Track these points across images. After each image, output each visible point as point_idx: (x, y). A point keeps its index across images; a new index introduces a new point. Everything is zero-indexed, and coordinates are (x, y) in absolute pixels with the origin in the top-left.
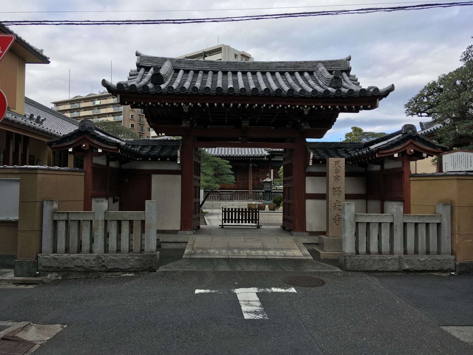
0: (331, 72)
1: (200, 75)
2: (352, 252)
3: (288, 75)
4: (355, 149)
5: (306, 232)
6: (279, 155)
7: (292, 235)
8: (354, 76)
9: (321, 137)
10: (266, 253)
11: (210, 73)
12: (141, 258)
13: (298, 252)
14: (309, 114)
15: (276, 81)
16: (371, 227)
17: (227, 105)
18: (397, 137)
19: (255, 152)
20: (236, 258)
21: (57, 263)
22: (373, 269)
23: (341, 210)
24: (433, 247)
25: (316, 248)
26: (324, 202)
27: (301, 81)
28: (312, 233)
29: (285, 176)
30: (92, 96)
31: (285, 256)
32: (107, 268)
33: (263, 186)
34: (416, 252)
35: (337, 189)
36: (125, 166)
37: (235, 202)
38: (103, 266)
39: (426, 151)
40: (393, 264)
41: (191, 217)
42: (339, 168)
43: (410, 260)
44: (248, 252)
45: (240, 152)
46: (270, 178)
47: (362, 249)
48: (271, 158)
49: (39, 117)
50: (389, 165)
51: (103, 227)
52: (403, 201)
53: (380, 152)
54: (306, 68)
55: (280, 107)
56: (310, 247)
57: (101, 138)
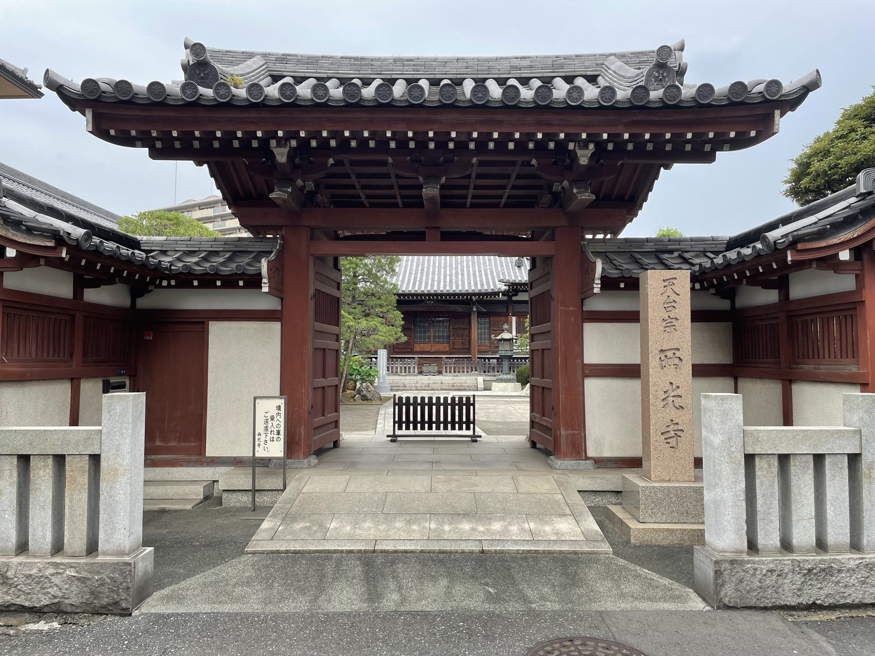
2: (740, 548)
4: (704, 253)
5: (587, 458)
13: (572, 529)
14: (588, 168)
16: (793, 469)
22: (804, 600)
26: (633, 385)
28: (602, 463)
30: (212, 199)
31: (533, 541)
35: (670, 354)
36: (143, 303)
42: (673, 297)
45: (454, 285)
46: (511, 333)
47: (769, 536)
48: (511, 297)
50: (803, 288)
53: (800, 246)
54: (580, 70)
56: (598, 500)
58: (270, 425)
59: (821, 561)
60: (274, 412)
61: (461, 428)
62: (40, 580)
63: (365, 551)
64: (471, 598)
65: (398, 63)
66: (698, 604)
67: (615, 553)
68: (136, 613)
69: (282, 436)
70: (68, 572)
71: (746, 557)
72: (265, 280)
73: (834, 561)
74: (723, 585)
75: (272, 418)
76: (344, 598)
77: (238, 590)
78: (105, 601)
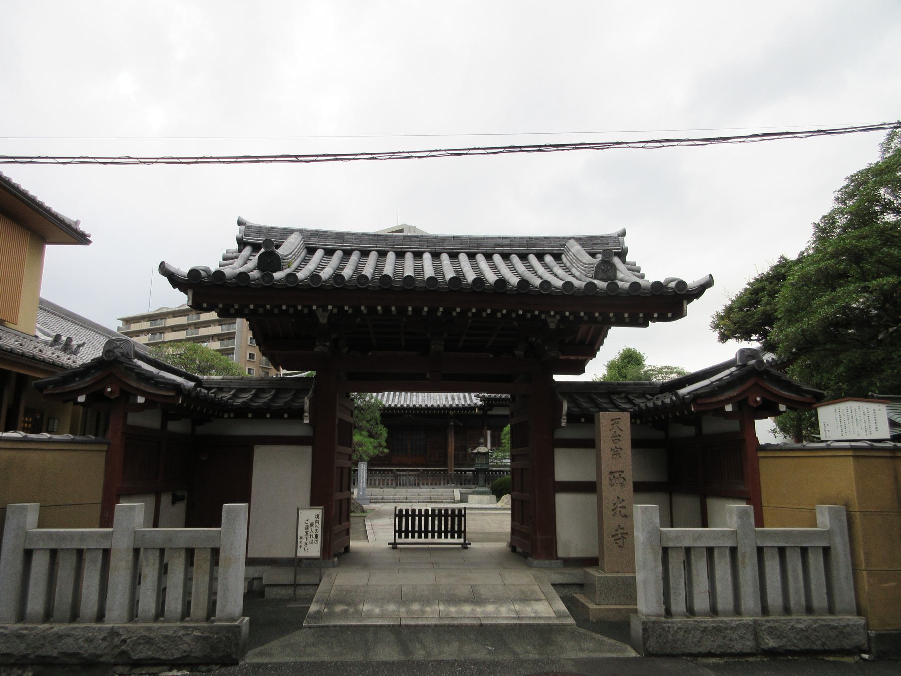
0: (593, 255)
1: (355, 257)
3: (515, 259)
5: (558, 558)
6: (497, 406)
7: (530, 566)
8: (634, 264)
9: (742, 351)
10: (478, 610)
11: (373, 256)
12: (206, 634)
13: (546, 609)
15: (494, 268)
16: (693, 558)
17: (402, 311)
18: (727, 372)
19: (459, 399)
20: (417, 626)
21: (22, 647)
22: (703, 650)
23: (628, 516)
24: (819, 599)
25: (580, 597)
26: (591, 498)
27: (540, 270)
28: (569, 562)
29: (513, 445)
31: (518, 618)
32: (130, 658)
33: (474, 460)
34: (787, 610)
35: (617, 475)
36: (201, 430)
37: (424, 490)
38: (123, 653)
39: (785, 400)
40: (742, 638)
41: (339, 519)
42: (619, 432)
43: (775, 628)
44: (442, 608)
46: (486, 446)
47: (679, 605)
49: (69, 340)
51: (130, 564)
52: (749, 501)
53: (699, 401)
54: (548, 249)
55: (502, 315)
56: (566, 591)
57: (143, 374)
58: (310, 530)
59: (713, 622)
60: (313, 520)
61: (453, 537)
62: (172, 640)
63: (393, 626)
64: (481, 653)
65: (407, 240)
66: (633, 654)
67: (578, 625)
68: (241, 663)
69: (319, 539)
70: (195, 633)
71: (663, 619)
72: (306, 414)
73: (722, 622)
74: (648, 638)
75: (312, 525)
76: (388, 653)
77: (308, 650)
78: (221, 654)
